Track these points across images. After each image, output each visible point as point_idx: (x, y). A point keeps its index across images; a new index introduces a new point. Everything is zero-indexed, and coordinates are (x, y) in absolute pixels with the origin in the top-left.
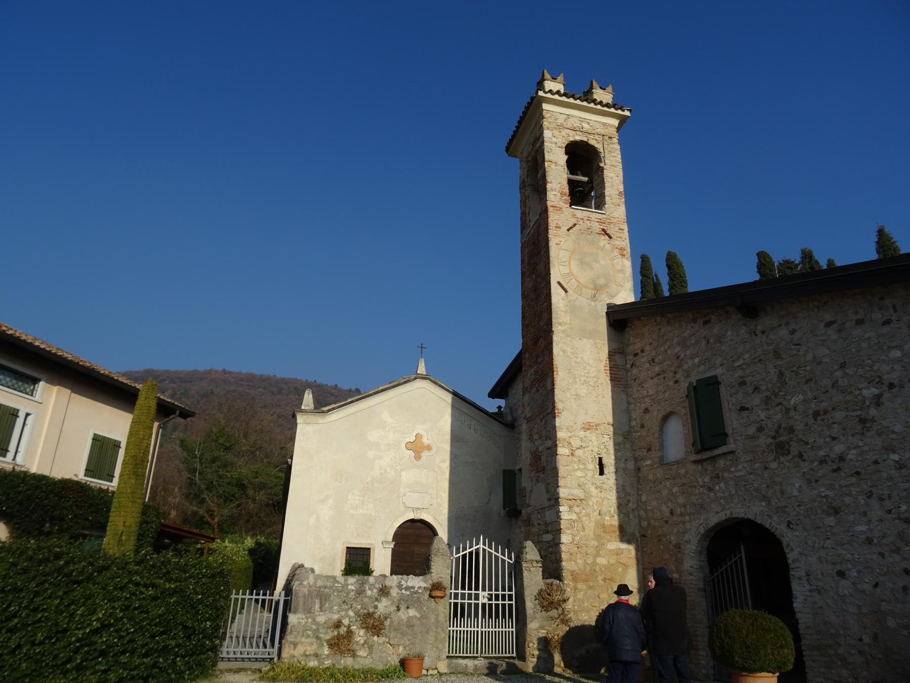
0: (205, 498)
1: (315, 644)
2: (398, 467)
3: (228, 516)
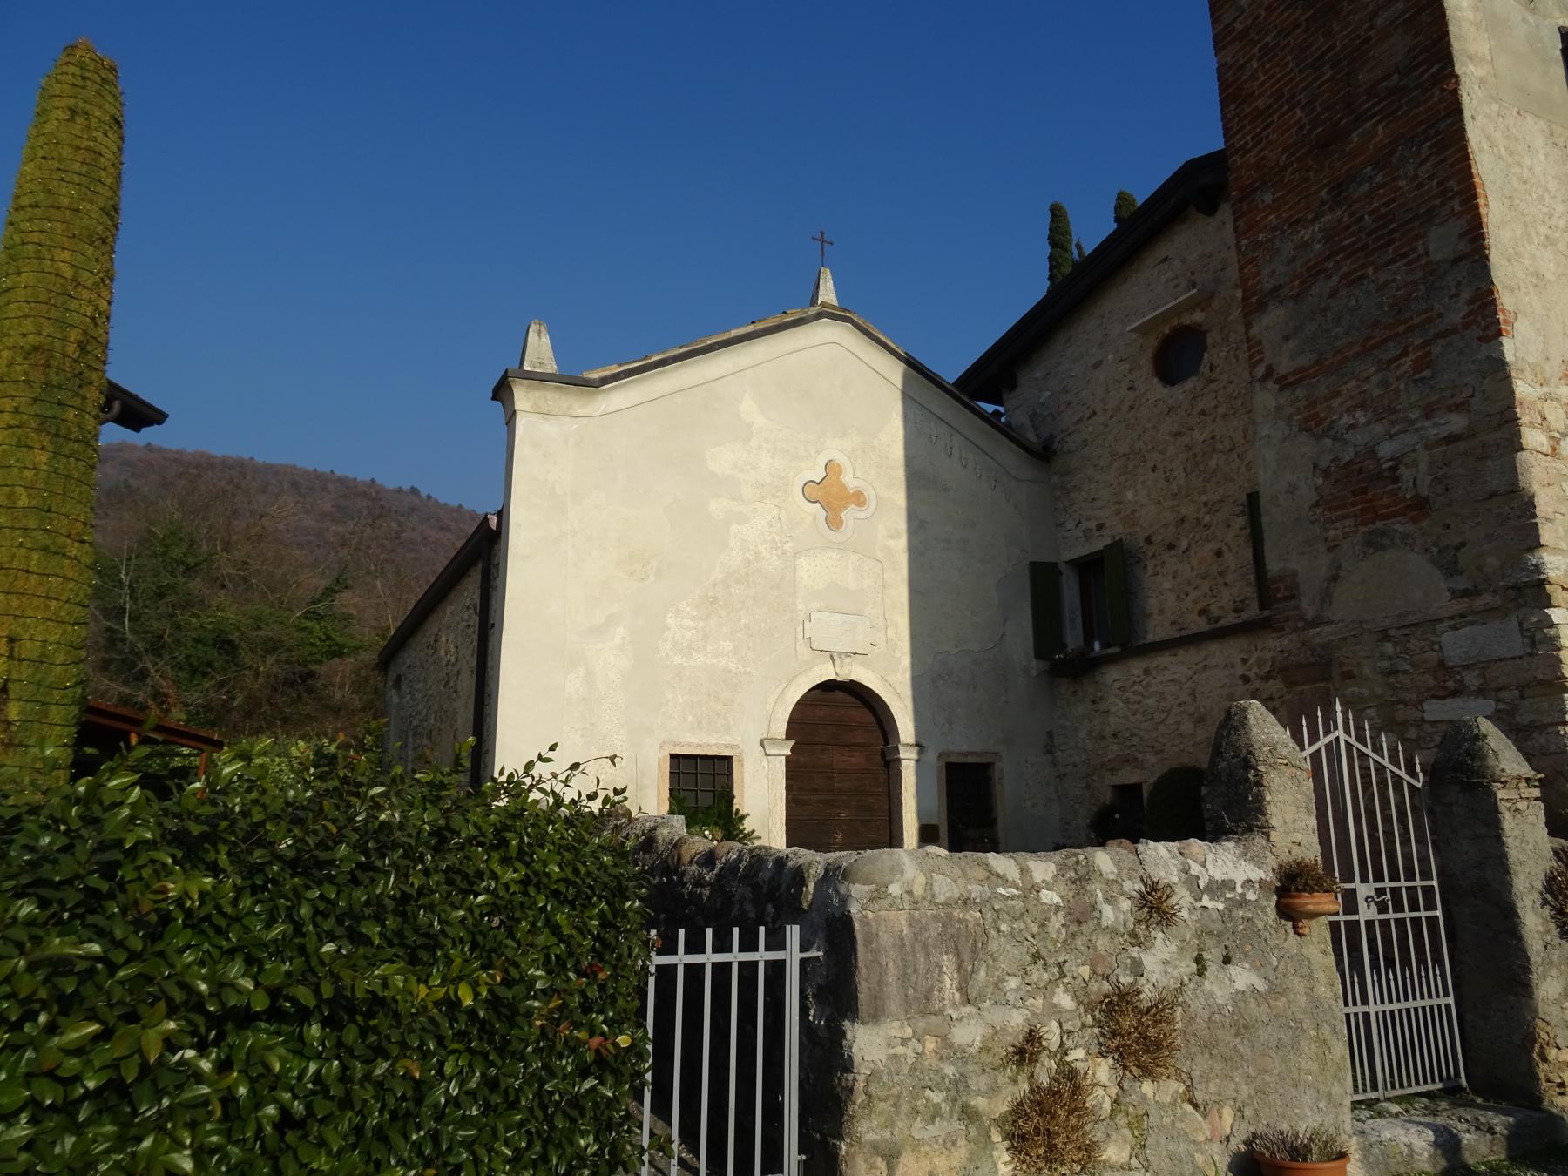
0: (147, 670)
1: (961, 1142)
2: (788, 546)
3: (199, 705)
